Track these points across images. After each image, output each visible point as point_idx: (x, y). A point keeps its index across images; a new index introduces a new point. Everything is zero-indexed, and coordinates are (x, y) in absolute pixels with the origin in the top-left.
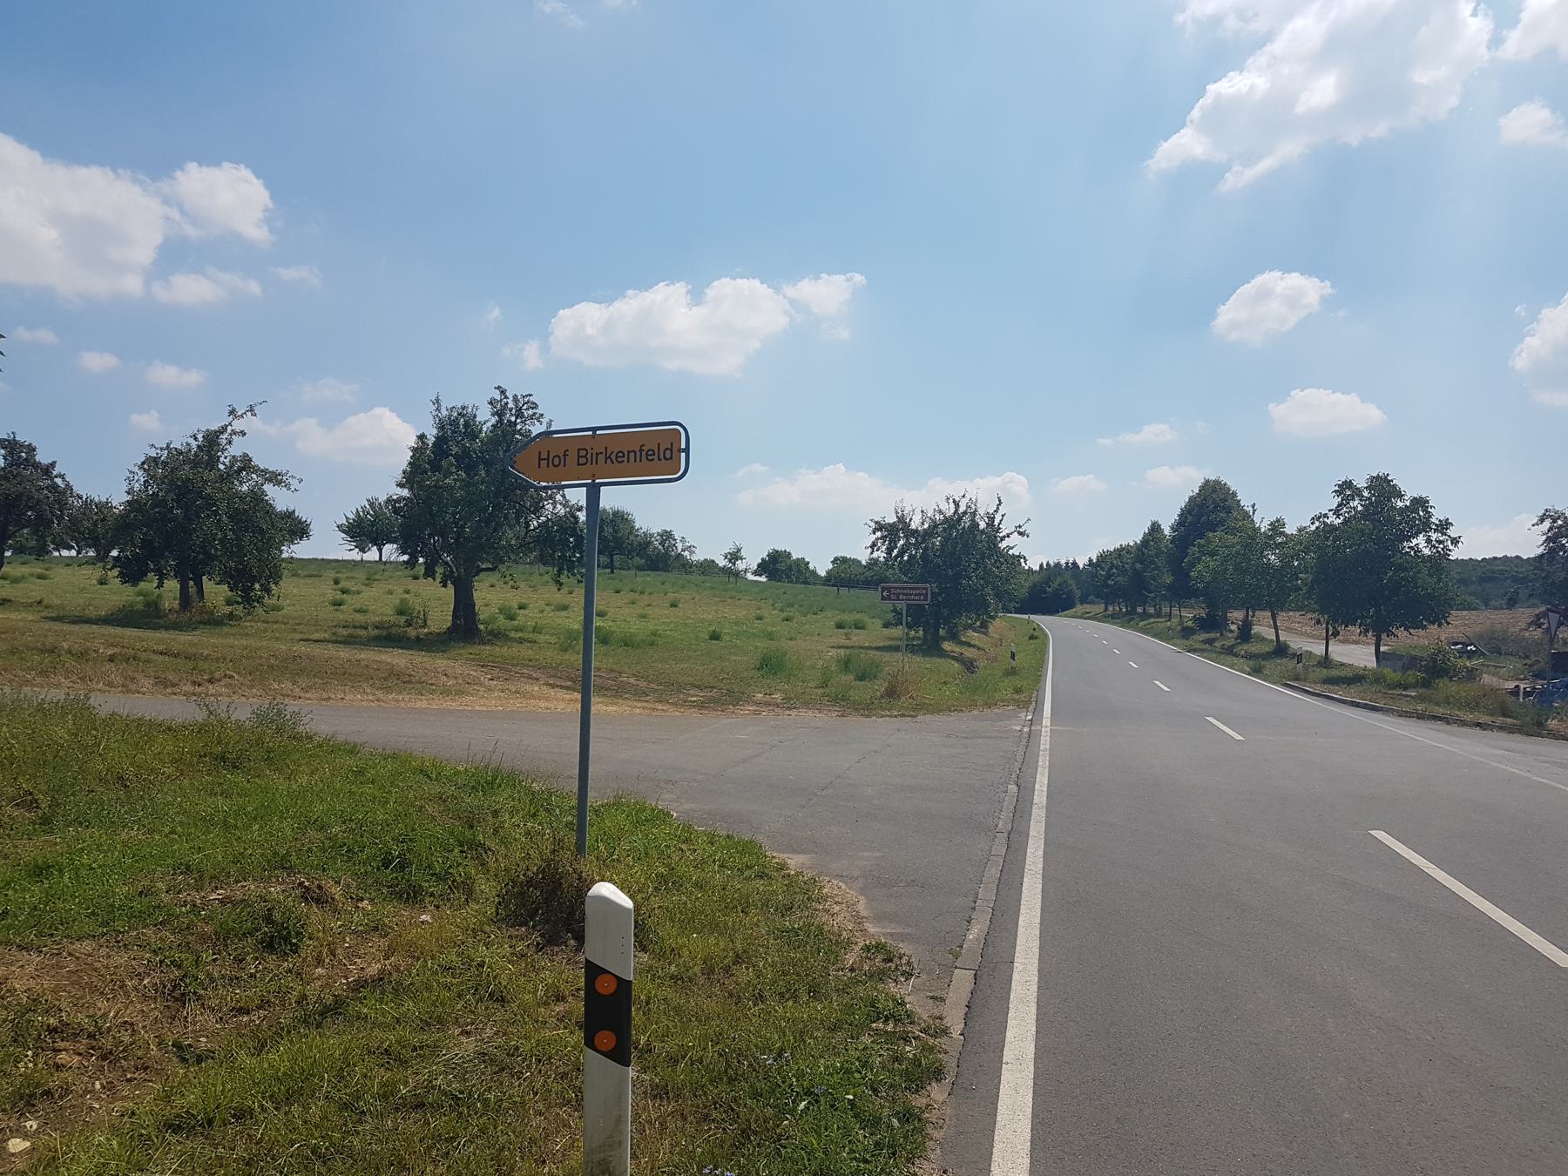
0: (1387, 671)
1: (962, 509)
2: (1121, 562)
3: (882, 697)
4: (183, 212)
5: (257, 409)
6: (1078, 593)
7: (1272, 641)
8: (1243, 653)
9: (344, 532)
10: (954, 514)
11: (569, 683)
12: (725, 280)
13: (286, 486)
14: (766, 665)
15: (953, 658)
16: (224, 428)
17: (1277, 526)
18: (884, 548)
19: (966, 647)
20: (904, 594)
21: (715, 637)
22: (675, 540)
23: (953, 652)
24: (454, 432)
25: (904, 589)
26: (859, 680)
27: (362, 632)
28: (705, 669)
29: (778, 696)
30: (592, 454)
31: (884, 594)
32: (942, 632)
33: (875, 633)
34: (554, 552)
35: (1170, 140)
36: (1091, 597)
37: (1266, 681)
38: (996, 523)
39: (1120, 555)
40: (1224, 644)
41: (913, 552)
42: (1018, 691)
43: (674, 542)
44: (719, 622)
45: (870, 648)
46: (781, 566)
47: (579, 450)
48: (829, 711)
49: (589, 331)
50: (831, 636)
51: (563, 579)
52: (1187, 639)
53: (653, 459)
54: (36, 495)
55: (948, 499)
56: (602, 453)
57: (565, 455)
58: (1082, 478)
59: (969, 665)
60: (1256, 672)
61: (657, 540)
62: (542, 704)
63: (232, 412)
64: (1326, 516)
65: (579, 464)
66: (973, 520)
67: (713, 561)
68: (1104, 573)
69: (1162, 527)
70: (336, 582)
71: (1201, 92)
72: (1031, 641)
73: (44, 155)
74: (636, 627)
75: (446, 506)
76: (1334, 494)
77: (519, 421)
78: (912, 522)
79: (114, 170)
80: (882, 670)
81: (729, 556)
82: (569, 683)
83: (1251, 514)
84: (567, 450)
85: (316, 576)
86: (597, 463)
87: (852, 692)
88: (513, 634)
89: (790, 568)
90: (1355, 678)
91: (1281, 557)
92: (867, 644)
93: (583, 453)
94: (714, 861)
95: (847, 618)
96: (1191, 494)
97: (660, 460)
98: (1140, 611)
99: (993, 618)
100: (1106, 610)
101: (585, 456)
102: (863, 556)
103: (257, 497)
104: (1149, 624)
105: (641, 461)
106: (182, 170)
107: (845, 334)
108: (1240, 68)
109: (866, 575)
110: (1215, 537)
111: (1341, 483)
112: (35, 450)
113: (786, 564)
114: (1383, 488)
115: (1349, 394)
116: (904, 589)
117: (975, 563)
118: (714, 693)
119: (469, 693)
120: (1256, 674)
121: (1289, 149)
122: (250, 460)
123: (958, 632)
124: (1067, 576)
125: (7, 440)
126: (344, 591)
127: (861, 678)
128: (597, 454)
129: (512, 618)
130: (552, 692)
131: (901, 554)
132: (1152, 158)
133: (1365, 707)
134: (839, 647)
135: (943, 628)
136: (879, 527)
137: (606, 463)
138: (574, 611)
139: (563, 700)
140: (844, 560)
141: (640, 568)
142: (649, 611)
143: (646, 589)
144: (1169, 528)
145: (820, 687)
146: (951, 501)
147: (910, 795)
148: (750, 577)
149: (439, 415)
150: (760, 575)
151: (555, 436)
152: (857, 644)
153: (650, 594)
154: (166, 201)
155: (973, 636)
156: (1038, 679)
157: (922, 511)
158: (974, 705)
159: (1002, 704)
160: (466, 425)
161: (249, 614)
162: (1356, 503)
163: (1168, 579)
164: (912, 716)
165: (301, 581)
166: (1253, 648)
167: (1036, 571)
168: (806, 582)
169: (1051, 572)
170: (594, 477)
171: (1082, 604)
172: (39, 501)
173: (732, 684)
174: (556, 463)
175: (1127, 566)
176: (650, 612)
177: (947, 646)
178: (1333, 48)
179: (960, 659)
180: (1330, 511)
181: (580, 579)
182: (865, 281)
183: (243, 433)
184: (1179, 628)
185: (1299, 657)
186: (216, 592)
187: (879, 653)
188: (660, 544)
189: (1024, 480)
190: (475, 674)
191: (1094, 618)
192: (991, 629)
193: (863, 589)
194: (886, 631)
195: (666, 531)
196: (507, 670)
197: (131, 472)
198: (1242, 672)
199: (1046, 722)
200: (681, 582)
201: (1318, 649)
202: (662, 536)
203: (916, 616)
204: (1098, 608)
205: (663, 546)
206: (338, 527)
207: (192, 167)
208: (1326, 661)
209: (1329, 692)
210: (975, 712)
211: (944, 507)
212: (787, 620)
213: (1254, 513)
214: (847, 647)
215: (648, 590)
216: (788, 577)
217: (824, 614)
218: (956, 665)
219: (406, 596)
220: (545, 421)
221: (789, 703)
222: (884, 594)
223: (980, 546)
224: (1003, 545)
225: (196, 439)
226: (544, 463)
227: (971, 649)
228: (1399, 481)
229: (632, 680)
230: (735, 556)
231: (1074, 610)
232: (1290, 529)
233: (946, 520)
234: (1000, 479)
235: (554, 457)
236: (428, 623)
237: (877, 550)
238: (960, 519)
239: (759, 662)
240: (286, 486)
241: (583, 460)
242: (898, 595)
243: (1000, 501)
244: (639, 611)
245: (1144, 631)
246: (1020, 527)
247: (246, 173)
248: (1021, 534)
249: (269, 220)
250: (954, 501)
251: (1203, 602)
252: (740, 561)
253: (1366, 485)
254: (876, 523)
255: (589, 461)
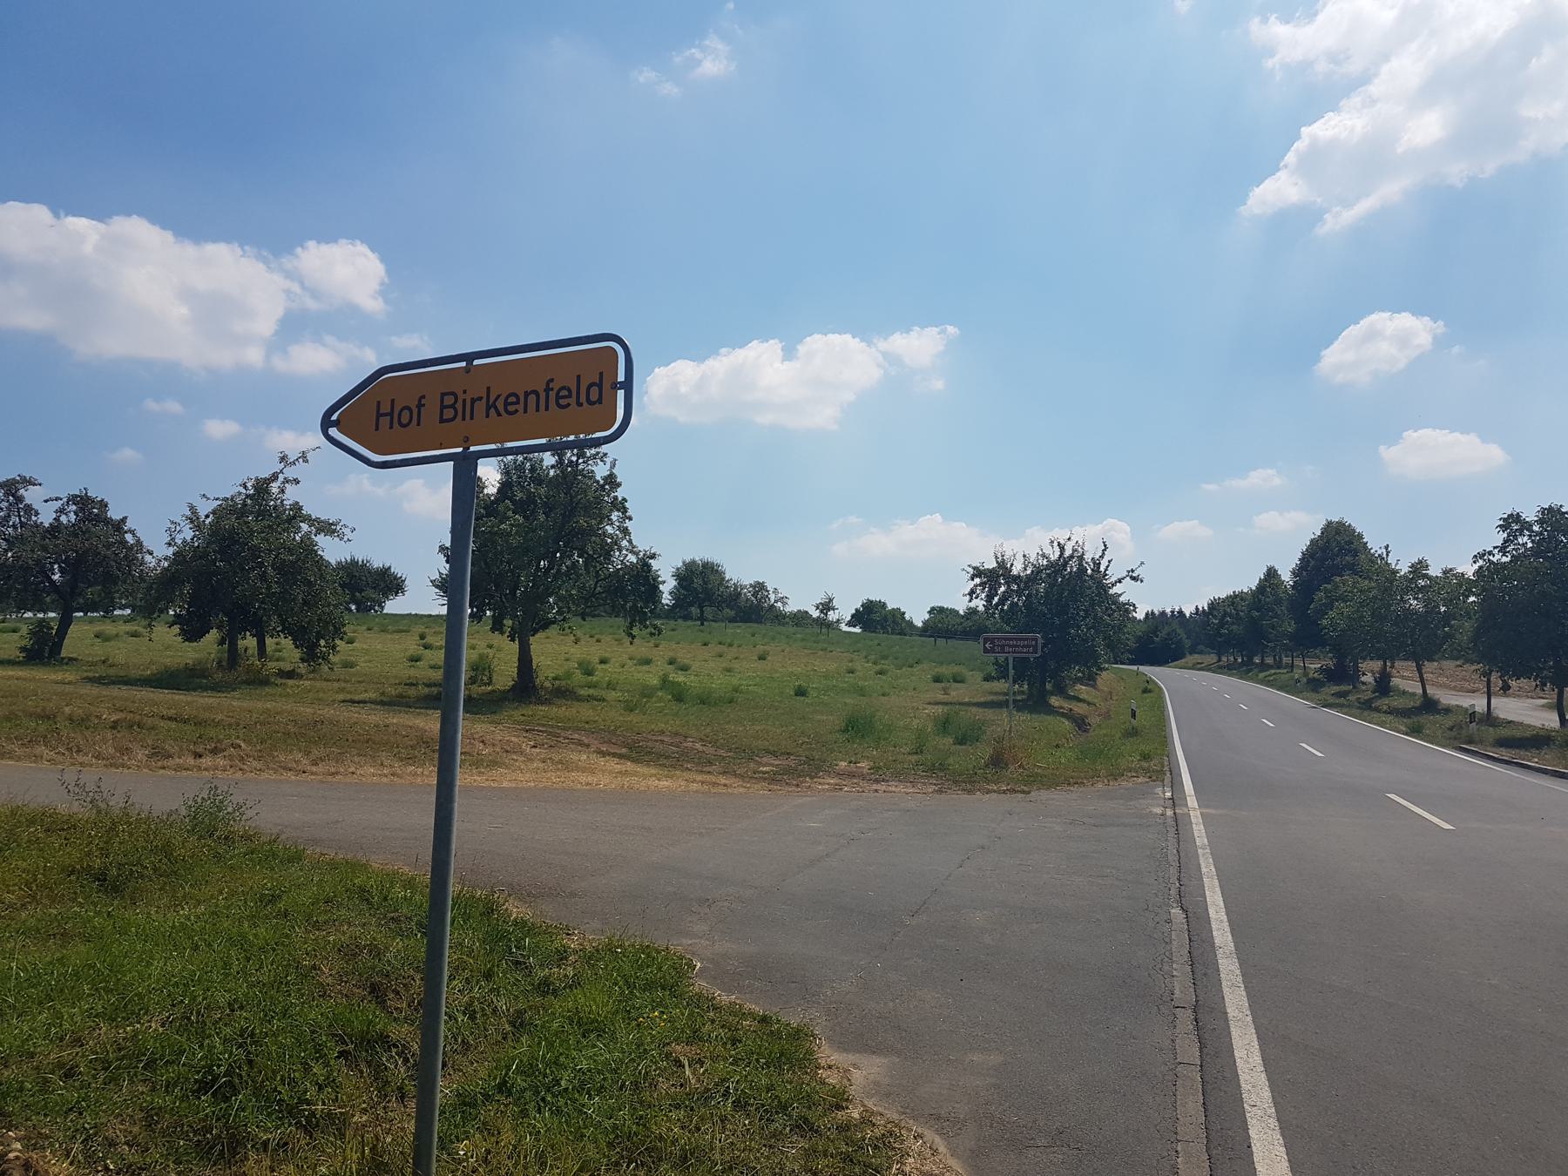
1: (1068, 553)
2: (1235, 609)
4: (302, 284)
5: (309, 456)
6: (1187, 643)
8: (1385, 708)
9: (437, 587)
10: (1059, 558)
11: (624, 750)
12: (816, 336)
13: (338, 536)
15: (1063, 715)
16: (275, 477)
17: (1419, 568)
18: (983, 595)
19: (1075, 703)
20: (1010, 646)
21: (801, 692)
22: (768, 591)
23: (1062, 708)
24: (520, 477)
28: (784, 731)
29: (864, 765)
30: (464, 401)
32: (1048, 686)
33: (975, 687)
34: (626, 602)
35: (1261, 186)
37: (1432, 744)
39: (1233, 603)
40: (1359, 698)
41: (1016, 600)
42: (1146, 757)
43: (766, 594)
46: (876, 617)
48: (924, 784)
49: (683, 389)
51: (635, 631)
52: (1317, 692)
53: (569, 405)
54: (103, 551)
55: (1052, 542)
56: (480, 399)
57: (420, 406)
59: (1081, 723)
60: (1415, 731)
61: (750, 592)
63: (283, 459)
64: (1490, 553)
65: (442, 421)
66: (1080, 565)
67: (807, 612)
69: (1279, 573)
70: (422, 637)
71: (1297, 137)
72: (1145, 695)
74: (719, 683)
75: (502, 553)
76: (1499, 529)
77: (581, 461)
79: (241, 246)
82: (624, 750)
83: (1385, 556)
84: (423, 397)
87: (951, 760)
88: (583, 692)
89: (885, 619)
90: (1537, 741)
91: (1427, 602)
92: (967, 700)
93: (449, 400)
95: (945, 670)
96: (1313, 537)
98: (1257, 661)
99: (1101, 669)
100: (1220, 660)
101: (453, 406)
102: (961, 605)
103: (309, 548)
104: (1270, 675)
105: (547, 409)
106: (302, 247)
107: (939, 385)
108: (1335, 108)
109: (964, 625)
111: (1506, 516)
112: (106, 506)
115: (1468, 434)
121: (1391, 190)
122: (300, 508)
123: (1066, 686)
124: (1175, 625)
126: (426, 647)
127: (961, 741)
128: (473, 401)
129: (589, 673)
130: (602, 761)
131: (1002, 602)
132: (1245, 204)
134: (937, 703)
135: (1050, 682)
136: (978, 572)
137: (487, 416)
138: (657, 666)
139: (610, 772)
140: (941, 610)
141: (732, 620)
142: (736, 665)
144: (1290, 573)
145: (914, 753)
146: (1055, 544)
147: (1035, 926)
148: (844, 628)
150: (855, 626)
151: (543, 441)
152: (955, 700)
154: (289, 275)
155: (1082, 690)
156: (1165, 741)
157: (1024, 556)
158: (1096, 775)
159: (1129, 774)
160: (533, 469)
161: (313, 671)
163: (1290, 627)
164: (1023, 792)
166: (1398, 702)
168: (902, 633)
169: (1157, 621)
170: (466, 442)
172: (105, 557)
173: (813, 749)
176: (737, 666)
177: (1055, 701)
178: (1436, 86)
179: (1069, 715)
180: (1495, 548)
182: (958, 332)
183: (297, 481)
184: (1305, 680)
186: (285, 649)
189: (1128, 529)
190: (516, 740)
191: (1208, 669)
192: (1099, 681)
193: (962, 639)
194: (987, 685)
196: (555, 736)
197: (172, 522)
198: (1398, 732)
199: (1192, 801)
201: (1480, 704)
203: (1022, 670)
204: (1211, 658)
206: (431, 581)
207: (311, 244)
208: (1489, 718)
209: (1520, 758)
210: (1100, 785)
211: (1049, 550)
212: (880, 674)
213: (1387, 555)
215: (736, 643)
216: (883, 628)
217: (919, 667)
218: (1067, 723)
219: (489, 650)
220: (608, 460)
221: (878, 774)
223: (1088, 592)
227: (1080, 704)
229: (698, 746)
230: (826, 607)
232: (1435, 571)
233: (1051, 565)
234: (1100, 525)
236: (494, 681)
237: (976, 598)
238: (1065, 564)
239: (844, 724)
240: (338, 536)
241: (449, 413)
243: (1105, 546)
244: (724, 665)
245: (1261, 682)
246: (1133, 571)
247: (362, 248)
248: (1133, 578)
249: (384, 292)
250: (1059, 544)
251: (1330, 652)
252: (832, 612)
253: (1536, 519)
254: (974, 568)
255: (460, 413)
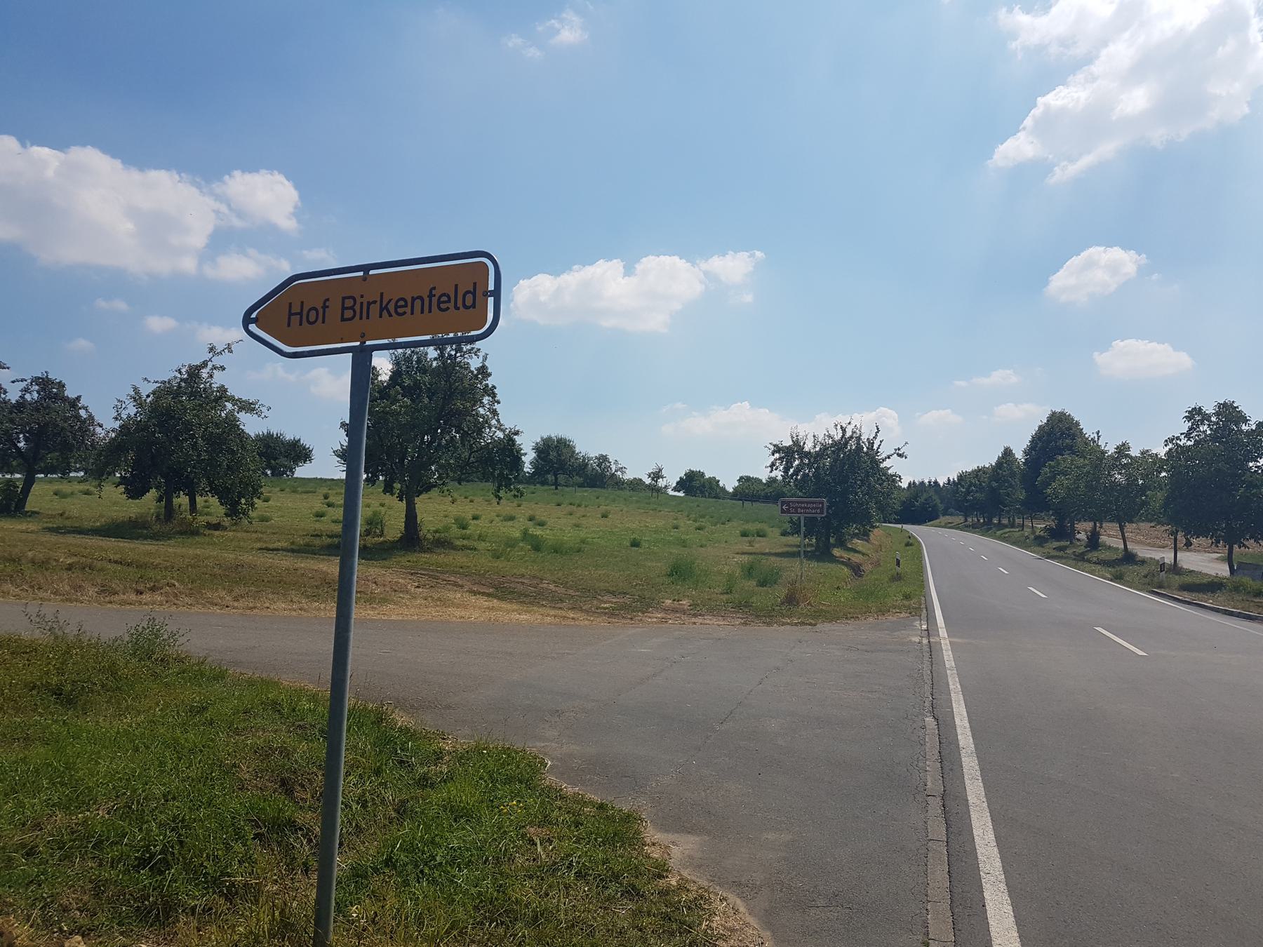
0: (1247, 580)
1: (848, 434)
2: (979, 481)
3: (782, 603)
4: (229, 206)
6: (941, 507)
7: (1117, 549)
8: (1095, 559)
12: (651, 258)
13: (257, 413)
14: (676, 573)
15: (843, 563)
16: (205, 364)
17: (1122, 449)
18: (781, 468)
20: (801, 508)
21: (635, 544)
23: (842, 557)
25: (802, 503)
26: (761, 586)
27: (317, 542)
30: (362, 303)
31: (784, 507)
32: (832, 540)
33: (775, 541)
34: (494, 470)
35: (1004, 144)
36: (951, 510)
37: (1131, 588)
38: (875, 447)
40: (1075, 552)
41: (807, 471)
42: (907, 597)
44: (642, 531)
45: (770, 554)
46: (696, 484)
47: (344, 299)
48: (733, 618)
49: (543, 298)
50: (736, 543)
51: (502, 494)
54: (61, 424)
55: (836, 425)
56: (375, 302)
57: (325, 307)
58: (942, 412)
59: (857, 570)
60: (1118, 578)
62: (458, 613)
63: (212, 349)
64: (1178, 438)
65: (343, 319)
66: (858, 444)
68: (964, 490)
69: (1014, 452)
70: (326, 497)
71: (1034, 105)
73: (123, 163)
74: (569, 536)
75: (392, 429)
76: (1185, 419)
77: (458, 355)
78: (806, 446)
80: (781, 576)
81: (652, 475)
85: (311, 492)
86: (368, 317)
87: (754, 599)
88: (458, 543)
89: (704, 486)
90: (1212, 586)
91: (1129, 476)
93: (349, 303)
94: (570, 866)
97: (457, 308)
100: (966, 521)
101: (352, 308)
102: (763, 475)
103: (232, 423)
105: (430, 311)
106: (229, 175)
108: (1064, 83)
110: (1065, 460)
111: (1190, 409)
112: (64, 386)
113: (700, 482)
114: (1229, 413)
116: (802, 503)
117: (860, 480)
118: (627, 600)
119: (393, 600)
120: (1119, 580)
121: (1107, 149)
122: (226, 391)
125: (41, 378)
126: (329, 505)
127: (762, 584)
128: (369, 304)
130: (473, 599)
133: (1238, 615)
134: (743, 553)
136: (777, 449)
137: (381, 317)
138: (519, 521)
140: (748, 479)
141: (581, 486)
142: (584, 521)
143: (583, 503)
146: (839, 427)
148: (671, 492)
149: (396, 353)
150: (679, 491)
151: (428, 337)
152: (758, 551)
153: (586, 507)
154: (218, 198)
155: (858, 543)
156: (923, 584)
157: (814, 436)
158: (867, 612)
159: (894, 611)
160: (419, 361)
162: (1206, 427)
164: (810, 624)
165: (298, 496)
167: (904, 489)
168: (716, 497)
169: (917, 489)
170: (363, 337)
171: (943, 516)
172: (63, 428)
174: (312, 319)
175: (984, 484)
177: (837, 552)
178: (1138, 71)
179: (848, 564)
180: (1181, 434)
181: (516, 494)
183: (223, 368)
185: (1143, 562)
186: (212, 506)
187: (778, 559)
188: (597, 466)
191: (956, 527)
192: (872, 536)
194: (784, 539)
195: (602, 456)
199: (943, 632)
200: (612, 497)
201: (1168, 557)
202: (599, 459)
203: (812, 527)
204: (959, 519)
205: (600, 468)
206: (334, 452)
207: (237, 173)
208: (1175, 568)
210: (871, 619)
211: (833, 432)
212: (699, 529)
213: (1098, 439)
214: (751, 554)
216: (702, 492)
220: (481, 354)
221: (696, 610)
222: (784, 507)
224: (882, 466)
225: (180, 373)
226: (295, 319)
228: (1244, 407)
229: (552, 587)
230: (657, 475)
231: (938, 521)
232: (1135, 452)
233: (835, 444)
235: (310, 310)
236: (385, 532)
237: (776, 469)
238: (846, 443)
240: (257, 413)
241: (349, 314)
242: (796, 509)
243: (878, 429)
245: (1000, 538)
246: (899, 449)
247: (280, 178)
248: (900, 455)
249: (297, 214)
250: (842, 427)
252: (661, 479)
254: (775, 446)
